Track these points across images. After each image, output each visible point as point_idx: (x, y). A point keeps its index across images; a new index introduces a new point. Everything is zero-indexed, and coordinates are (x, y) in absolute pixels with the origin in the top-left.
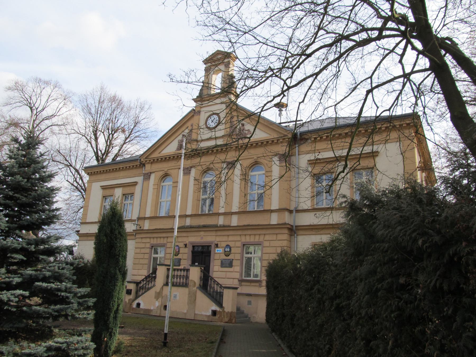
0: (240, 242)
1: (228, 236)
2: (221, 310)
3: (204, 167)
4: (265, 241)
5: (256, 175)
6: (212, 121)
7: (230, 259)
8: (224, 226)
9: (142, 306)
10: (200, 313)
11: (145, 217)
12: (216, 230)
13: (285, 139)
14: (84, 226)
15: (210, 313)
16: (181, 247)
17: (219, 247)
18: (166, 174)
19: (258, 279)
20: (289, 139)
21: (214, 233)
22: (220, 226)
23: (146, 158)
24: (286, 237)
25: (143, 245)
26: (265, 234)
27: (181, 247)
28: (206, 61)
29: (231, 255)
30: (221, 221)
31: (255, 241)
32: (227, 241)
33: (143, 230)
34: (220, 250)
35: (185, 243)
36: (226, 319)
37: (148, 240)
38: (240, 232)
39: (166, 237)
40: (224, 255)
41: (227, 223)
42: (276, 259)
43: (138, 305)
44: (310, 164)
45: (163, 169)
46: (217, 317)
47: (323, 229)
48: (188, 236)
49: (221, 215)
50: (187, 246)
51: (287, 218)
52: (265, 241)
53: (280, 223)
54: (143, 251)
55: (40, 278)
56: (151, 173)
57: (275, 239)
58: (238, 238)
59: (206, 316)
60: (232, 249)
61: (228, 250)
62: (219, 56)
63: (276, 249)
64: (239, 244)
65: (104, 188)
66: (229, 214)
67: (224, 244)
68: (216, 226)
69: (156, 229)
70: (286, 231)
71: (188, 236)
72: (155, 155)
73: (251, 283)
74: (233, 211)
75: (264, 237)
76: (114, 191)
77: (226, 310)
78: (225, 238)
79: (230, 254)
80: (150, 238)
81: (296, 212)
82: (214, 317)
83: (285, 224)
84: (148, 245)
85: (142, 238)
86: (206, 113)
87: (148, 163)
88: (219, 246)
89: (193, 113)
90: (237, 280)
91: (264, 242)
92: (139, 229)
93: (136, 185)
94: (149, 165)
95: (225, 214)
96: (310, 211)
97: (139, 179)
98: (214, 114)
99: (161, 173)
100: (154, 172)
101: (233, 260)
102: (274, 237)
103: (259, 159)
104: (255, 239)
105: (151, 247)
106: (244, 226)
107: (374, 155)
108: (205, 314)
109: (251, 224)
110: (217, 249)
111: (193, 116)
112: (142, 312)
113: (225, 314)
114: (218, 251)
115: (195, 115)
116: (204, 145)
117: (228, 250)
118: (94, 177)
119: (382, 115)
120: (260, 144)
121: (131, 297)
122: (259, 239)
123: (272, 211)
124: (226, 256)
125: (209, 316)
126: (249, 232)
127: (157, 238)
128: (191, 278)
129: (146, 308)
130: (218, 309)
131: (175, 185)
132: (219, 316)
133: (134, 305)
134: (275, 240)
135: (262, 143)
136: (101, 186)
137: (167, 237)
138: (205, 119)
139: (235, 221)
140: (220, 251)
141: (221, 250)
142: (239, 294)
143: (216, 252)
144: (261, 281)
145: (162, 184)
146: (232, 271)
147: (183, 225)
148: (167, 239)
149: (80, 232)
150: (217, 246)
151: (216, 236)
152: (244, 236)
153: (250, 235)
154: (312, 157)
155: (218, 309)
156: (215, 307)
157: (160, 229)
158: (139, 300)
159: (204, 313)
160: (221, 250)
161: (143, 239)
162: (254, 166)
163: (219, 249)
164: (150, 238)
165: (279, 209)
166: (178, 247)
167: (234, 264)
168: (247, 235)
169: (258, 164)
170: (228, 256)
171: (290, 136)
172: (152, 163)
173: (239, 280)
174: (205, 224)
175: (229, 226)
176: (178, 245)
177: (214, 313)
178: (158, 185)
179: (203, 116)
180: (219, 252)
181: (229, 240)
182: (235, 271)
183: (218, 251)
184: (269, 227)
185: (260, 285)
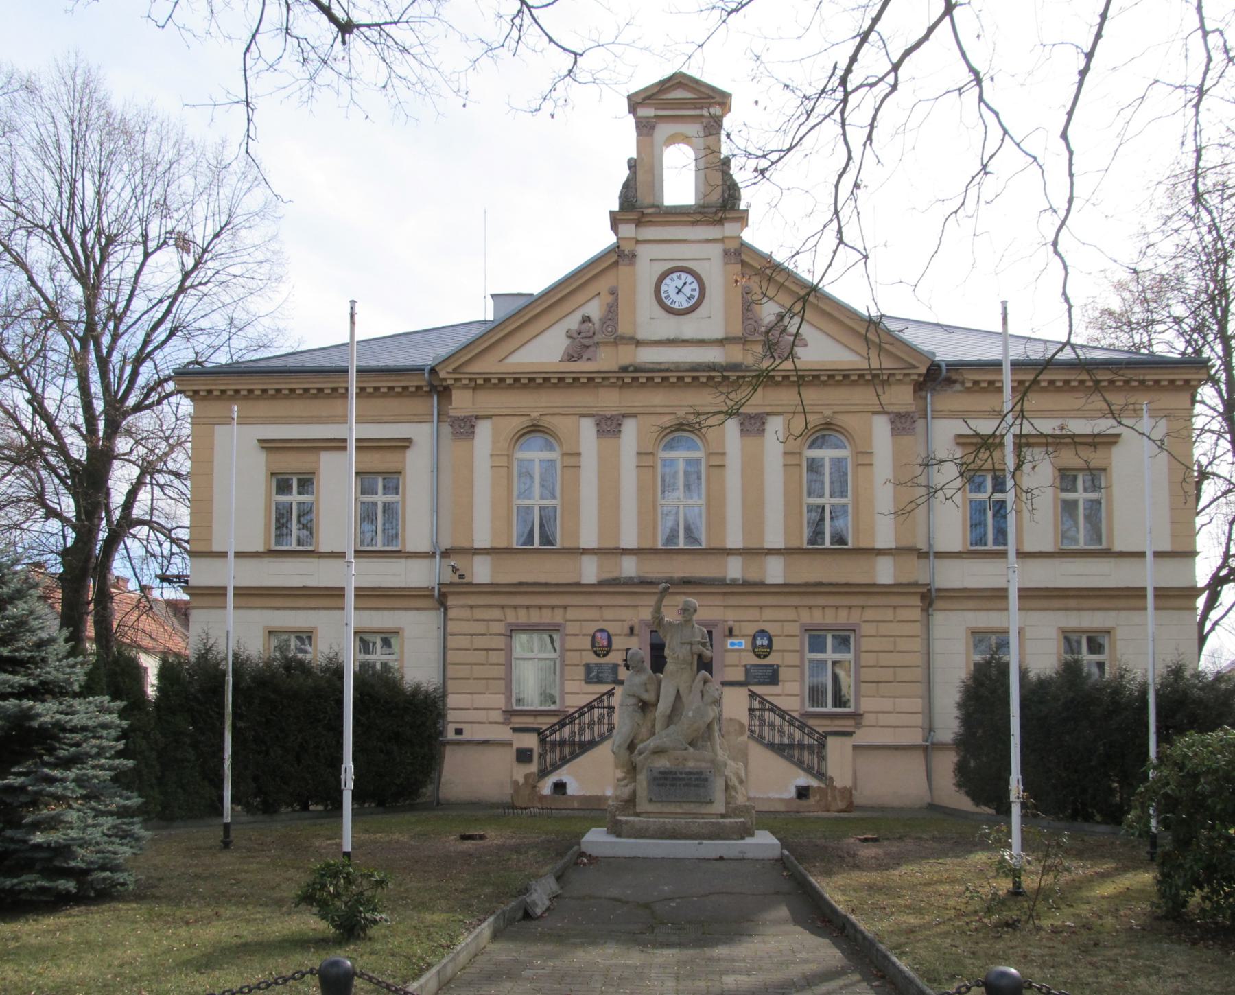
0: (798, 624)
1: (761, 607)
2: (823, 786)
3: (814, 420)
4: (865, 622)
5: (677, 459)
6: (680, 291)
7: (772, 666)
8: (746, 583)
9: (572, 789)
10: (765, 796)
11: (473, 549)
12: (725, 593)
13: (909, 375)
14: (205, 563)
15: (792, 793)
16: (616, 635)
17: (736, 636)
18: (533, 426)
19: (851, 710)
20: (919, 375)
21: (718, 600)
22: (734, 583)
23: (455, 371)
24: (916, 614)
25: (480, 628)
26: (863, 607)
27: (616, 635)
28: (635, 103)
29: (772, 654)
30: (734, 569)
31: (839, 622)
32: (757, 621)
33: (470, 584)
34: (740, 644)
35: (631, 623)
36: (839, 803)
37: (497, 613)
38: (795, 600)
39: (535, 606)
40: (752, 654)
41: (753, 576)
42: (976, 664)
43: (560, 787)
44: (958, 444)
45: (526, 411)
46: (812, 801)
47: (1089, 597)
48: (637, 606)
49: (733, 554)
50: (636, 631)
51: (917, 572)
52: (865, 622)
53: (905, 580)
54: (480, 642)
55: (68, 727)
56: (477, 417)
57: (891, 618)
58: (790, 614)
59: (781, 800)
60: (774, 639)
61: (765, 642)
62: (679, 94)
63: (895, 642)
64: (794, 629)
65: (269, 446)
66: (753, 553)
67: (752, 629)
68: (722, 582)
69: (521, 584)
70: (917, 601)
71: (637, 606)
72: (488, 365)
73: (535, 716)
74: (624, 545)
75: (849, 614)
76: (404, 458)
77: (838, 783)
78: (752, 614)
79: (769, 653)
80: (503, 607)
81: (935, 557)
82: (804, 803)
83: (916, 584)
84: (498, 628)
85: (471, 607)
86: (653, 263)
87: (465, 387)
88: (735, 632)
89: (617, 258)
90: (500, 711)
91: (864, 625)
92: (456, 580)
93: (408, 447)
94: (468, 394)
95: (746, 552)
96: (964, 555)
97: (422, 433)
98: (689, 271)
99: (517, 423)
100: (489, 417)
101: (778, 666)
102: (889, 614)
103: (544, 418)
104: (836, 618)
105: (509, 633)
106: (807, 585)
107: (1111, 440)
108: (777, 796)
109: (825, 580)
110: (729, 641)
111: (616, 263)
112: (576, 805)
113: (837, 793)
114: (733, 644)
115: (621, 262)
116: (648, 356)
117: (765, 642)
118: (214, 409)
119: (1056, 357)
120: (840, 378)
121: (533, 768)
122: (848, 619)
123: (585, 551)
124: (758, 656)
125: (791, 800)
126: (821, 601)
127: (528, 607)
128: (727, 713)
129: (589, 794)
130: (814, 783)
131: (570, 461)
132: (818, 798)
133: (546, 787)
134: (891, 622)
135: (846, 377)
136: (260, 441)
137: (565, 607)
138: (654, 282)
139: (775, 571)
140: (740, 644)
141: (743, 641)
142: (855, 747)
143: (729, 647)
144: (861, 715)
145: (519, 454)
146: (780, 692)
147: (615, 575)
148: (565, 612)
149: (190, 584)
150: (731, 633)
151: (725, 606)
152: (833, 610)
153: (824, 607)
154: (960, 427)
155: (814, 783)
156: (803, 780)
157: (546, 584)
158: (563, 775)
159: (774, 795)
160: (743, 641)
161: (475, 611)
162: (527, 437)
163: (736, 641)
164: (503, 607)
165: (897, 549)
166: (605, 635)
167: (781, 677)
168: (843, 606)
169: (546, 433)
170: (765, 656)
171: (923, 370)
172: (476, 388)
173: (505, 712)
174: (687, 575)
175: (578, 584)
176: (606, 628)
177: (803, 793)
178: (508, 455)
179: (646, 270)
180: (736, 647)
181: (764, 618)
182: (786, 692)
183: (733, 644)
184: (576, 588)
185: (857, 724)
